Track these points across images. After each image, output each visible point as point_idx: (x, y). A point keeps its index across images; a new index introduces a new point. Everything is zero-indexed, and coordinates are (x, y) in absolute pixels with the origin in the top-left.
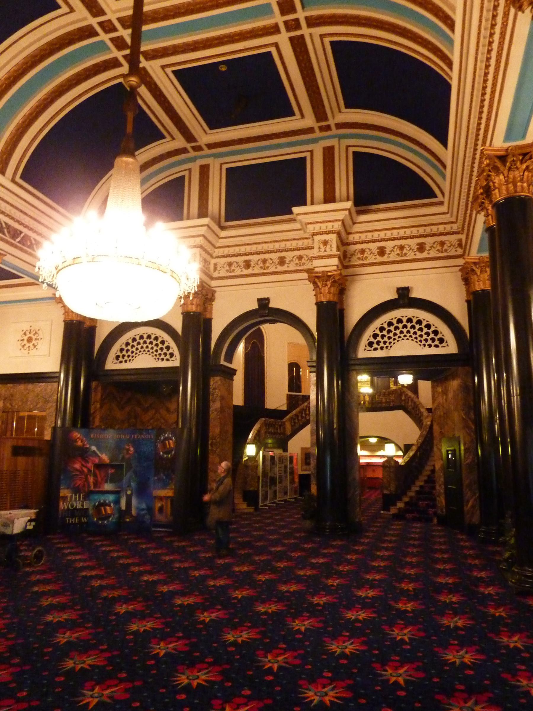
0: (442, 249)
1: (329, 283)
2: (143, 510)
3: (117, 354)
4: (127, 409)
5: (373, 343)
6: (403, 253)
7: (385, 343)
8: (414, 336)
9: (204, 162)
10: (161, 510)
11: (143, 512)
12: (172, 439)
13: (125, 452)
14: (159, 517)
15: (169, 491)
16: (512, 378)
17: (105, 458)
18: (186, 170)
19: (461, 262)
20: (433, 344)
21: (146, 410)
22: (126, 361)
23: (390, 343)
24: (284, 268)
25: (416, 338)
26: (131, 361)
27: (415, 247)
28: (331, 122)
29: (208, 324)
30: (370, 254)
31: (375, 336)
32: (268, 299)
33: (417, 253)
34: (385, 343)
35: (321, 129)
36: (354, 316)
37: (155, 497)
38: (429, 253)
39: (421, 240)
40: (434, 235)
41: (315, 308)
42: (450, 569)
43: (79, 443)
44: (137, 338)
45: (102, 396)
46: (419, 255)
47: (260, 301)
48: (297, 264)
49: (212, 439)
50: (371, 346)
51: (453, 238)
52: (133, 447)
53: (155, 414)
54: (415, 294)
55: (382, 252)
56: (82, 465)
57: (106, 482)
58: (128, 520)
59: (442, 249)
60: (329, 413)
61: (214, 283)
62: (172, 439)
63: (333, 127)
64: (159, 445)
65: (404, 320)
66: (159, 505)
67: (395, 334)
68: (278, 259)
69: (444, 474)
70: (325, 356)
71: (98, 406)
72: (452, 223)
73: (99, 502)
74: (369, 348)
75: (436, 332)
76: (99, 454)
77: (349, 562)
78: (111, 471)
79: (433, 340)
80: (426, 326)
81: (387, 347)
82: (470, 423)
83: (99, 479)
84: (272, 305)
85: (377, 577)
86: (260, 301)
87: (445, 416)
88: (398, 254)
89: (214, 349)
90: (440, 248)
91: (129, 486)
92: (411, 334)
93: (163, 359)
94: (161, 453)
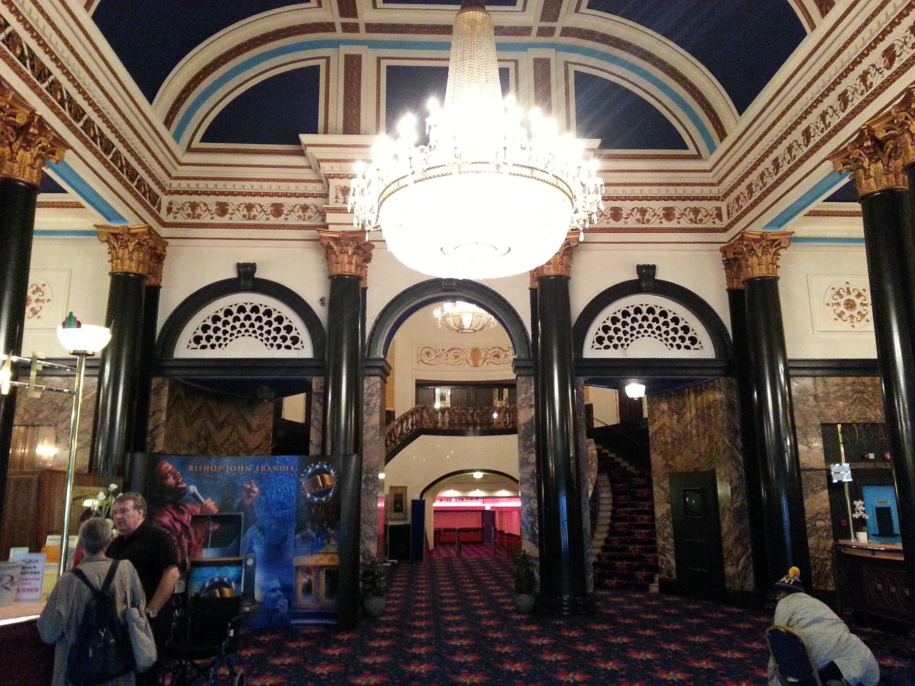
0: (696, 218)
1: (131, 246)
2: (274, 590)
3: (197, 334)
4: (198, 423)
5: (201, 338)
6: (646, 218)
7: (619, 339)
8: (251, 330)
9: (354, 50)
10: (308, 589)
11: (273, 595)
12: (329, 473)
13: (244, 493)
14: (305, 602)
15: (322, 556)
16: (897, 394)
17: (211, 505)
18: (511, 61)
19: (725, 237)
20: (683, 345)
21: (220, 426)
22: (213, 347)
23: (225, 339)
24: (225, 220)
25: (261, 335)
26: (223, 346)
27: (661, 213)
28: (559, 25)
29: (154, 292)
30: (706, 216)
31: (606, 329)
32: (253, 267)
33: (663, 220)
34: (619, 339)
35: (346, 28)
36: (580, 300)
37: (297, 568)
38: (679, 223)
39: (276, 200)
40: (186, 193)
41: (108, 280)
42: (473, 662)
43: (171, 481)
44: (234, 310)
45: (169, 401)
46: (666, 224)
47: (640, 268)
48: (299, 217)
49: (367, 473)
50: (601, 343)
51: (710, 205)
52: (257, 485)
53: (231, 434)
54: (661, 275)
55: (277, 210)
56: (174, 518)
57: (205, 546)
58: (247, 609)
59: (696, 218)
60: (562, 434)
61: (164, 232)
62: (329, 473)
63: (362, 28)
64: (304, 483)
65: (234, 309)
66: (302, 580)
67: (233, 328)
68: (611, 209)
69: (673, 522)
70: (555, 352)
71: (164, 418)
72: (712, 185)
73: (212, 580)
74: (598, 346)
75: (686, 329)
76: (203, 500)
77: (330, 660)
78: (214, 527)
79: (284, 339)
80: (276, 320)
81: (622, 345)
82: (736, 452)
83: (194, 542)
84: (659, 276)
85: (379, 660)
86: (640, 268)
87: (676, 442)
88: (638, 220)
89: (161, 334)
90: (693, 217)
91: (251, 551)
92: (238, 329)
93: (279, 347)
94: (308, 495)
